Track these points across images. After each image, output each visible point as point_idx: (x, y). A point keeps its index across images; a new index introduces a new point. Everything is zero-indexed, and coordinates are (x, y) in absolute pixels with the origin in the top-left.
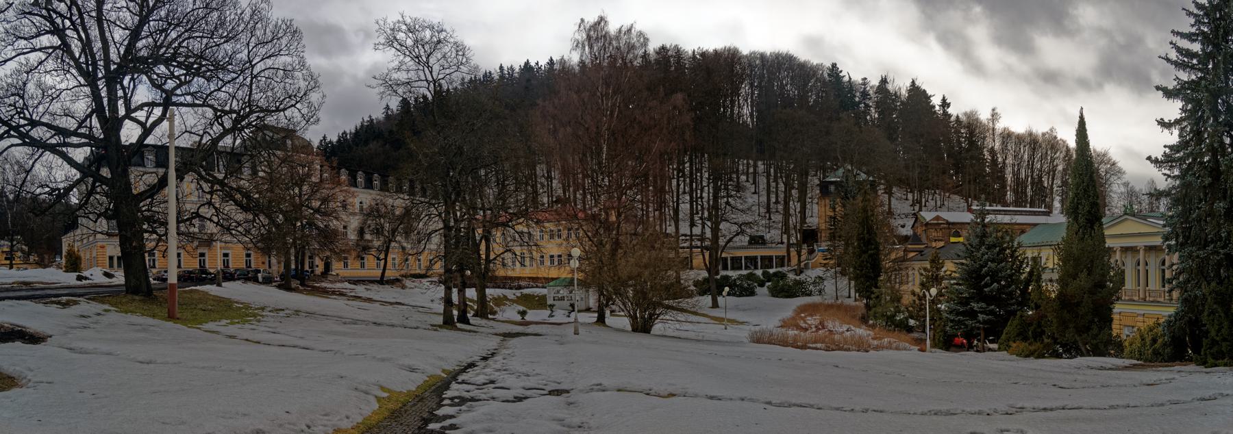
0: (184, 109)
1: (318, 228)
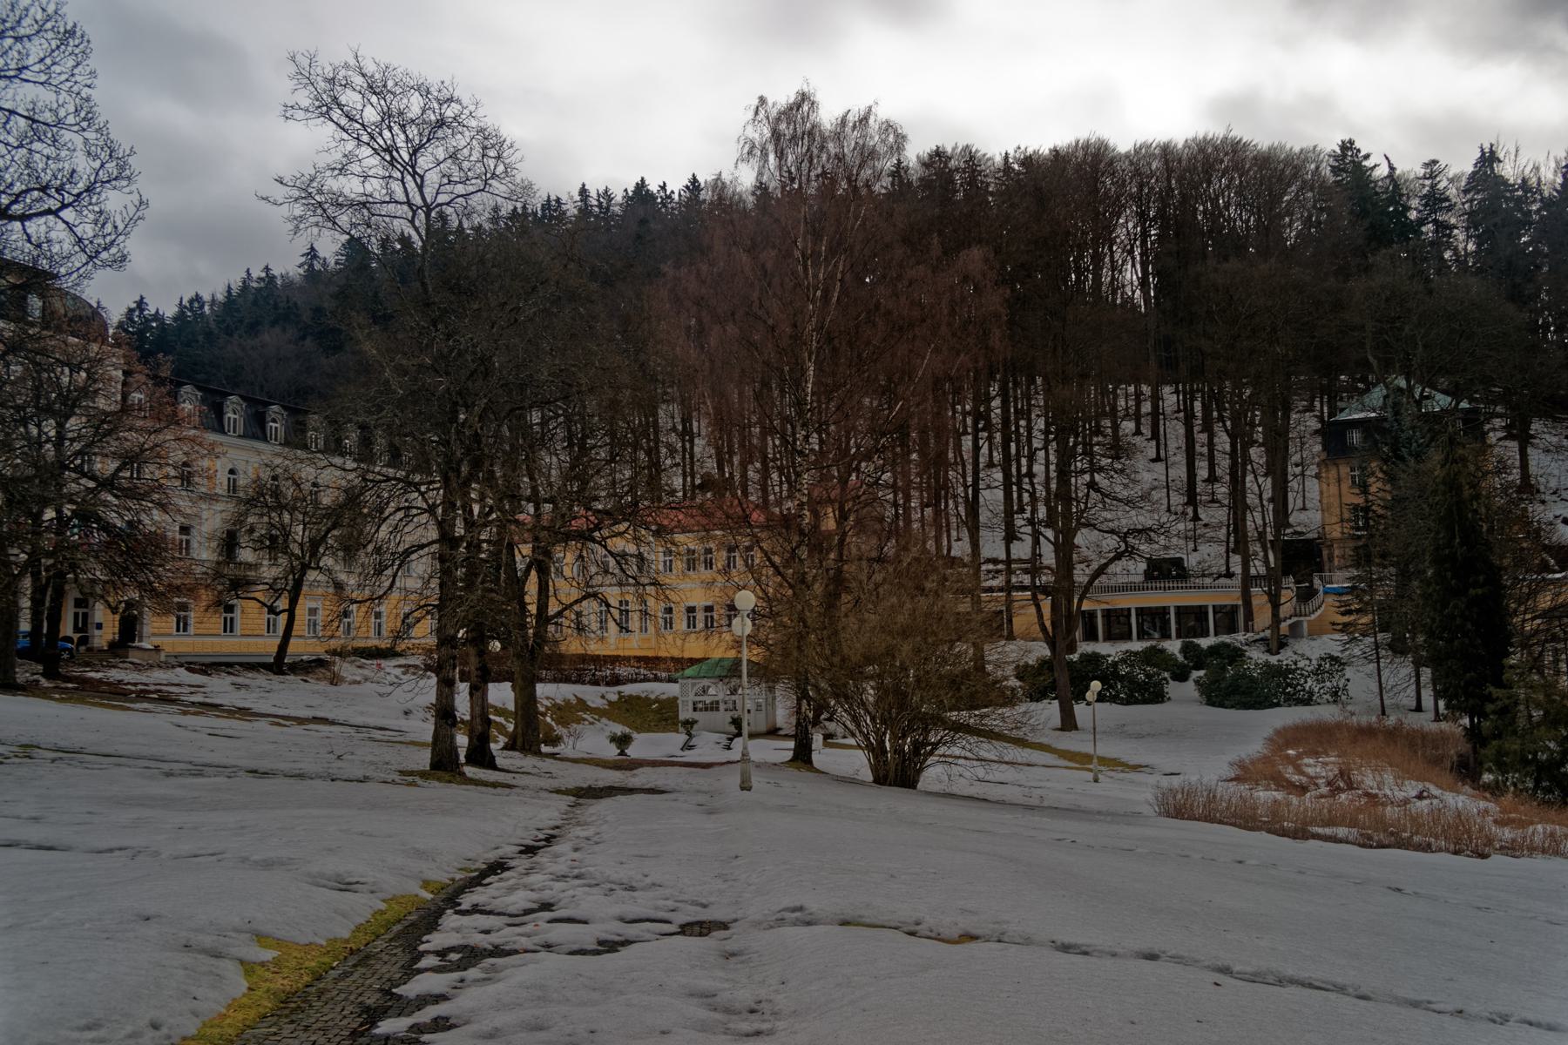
1: (106, 527)
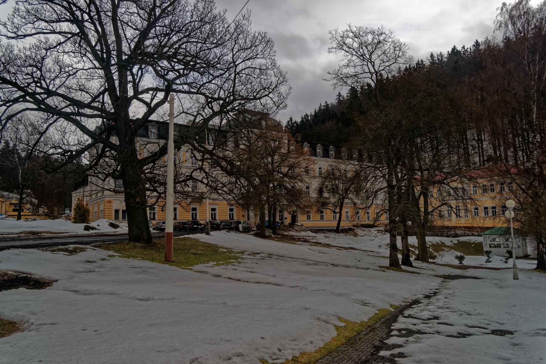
0: (182, 95)
1: (286, 188)
